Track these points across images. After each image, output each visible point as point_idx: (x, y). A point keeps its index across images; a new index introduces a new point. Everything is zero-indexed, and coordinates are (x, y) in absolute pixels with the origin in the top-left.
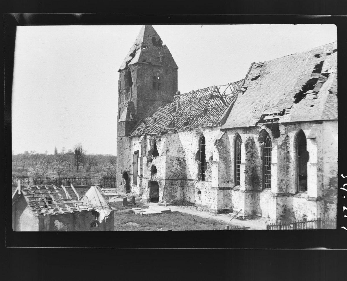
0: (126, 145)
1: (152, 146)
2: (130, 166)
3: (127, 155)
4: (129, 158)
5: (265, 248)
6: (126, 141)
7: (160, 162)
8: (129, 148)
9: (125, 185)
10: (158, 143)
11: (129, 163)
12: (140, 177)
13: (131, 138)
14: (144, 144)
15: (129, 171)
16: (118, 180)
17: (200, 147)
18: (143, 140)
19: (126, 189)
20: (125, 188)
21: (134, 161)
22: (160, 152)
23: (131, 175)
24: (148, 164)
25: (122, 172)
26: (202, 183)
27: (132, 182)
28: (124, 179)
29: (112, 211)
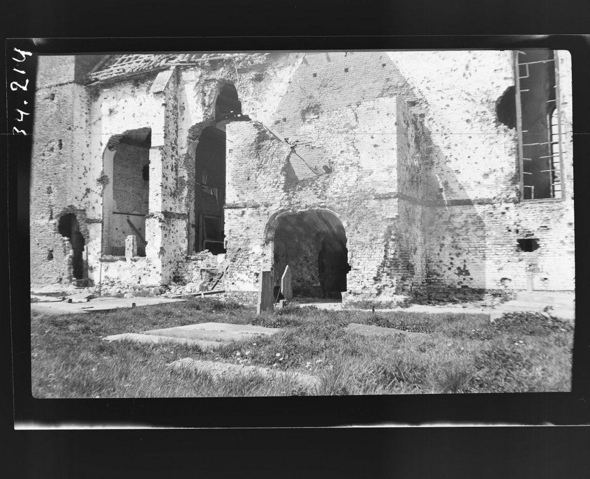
0: (77, 114)
1: (209, 106)
2: (88, 190)
3: (78, 151)
4: (85, 163)
5: (580, 424)
6: (78, 100)
7: (353, 128)
8: (84, 125)
9: (71, 257)
10: (251, 89)
11: (84, 180)
12: (160, 220)
13: (94, 93)
14: (172, 102)
15: (84, 210)
16: (481, 53)
17: (515, 73)
18: (171, 85)
19: (74, 272)
20: (72, 270)
21: (106, 174)
22: (54, 218)
23: (91, 221)
24: (259, 148)
25: (57, 211)
26: (188, 288)
27: (99, 249)
28: (66, 238)
29: (337, 298)
